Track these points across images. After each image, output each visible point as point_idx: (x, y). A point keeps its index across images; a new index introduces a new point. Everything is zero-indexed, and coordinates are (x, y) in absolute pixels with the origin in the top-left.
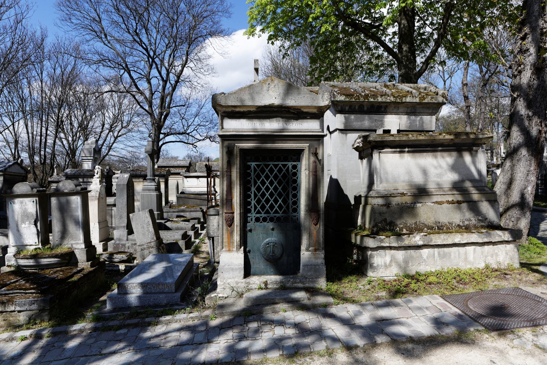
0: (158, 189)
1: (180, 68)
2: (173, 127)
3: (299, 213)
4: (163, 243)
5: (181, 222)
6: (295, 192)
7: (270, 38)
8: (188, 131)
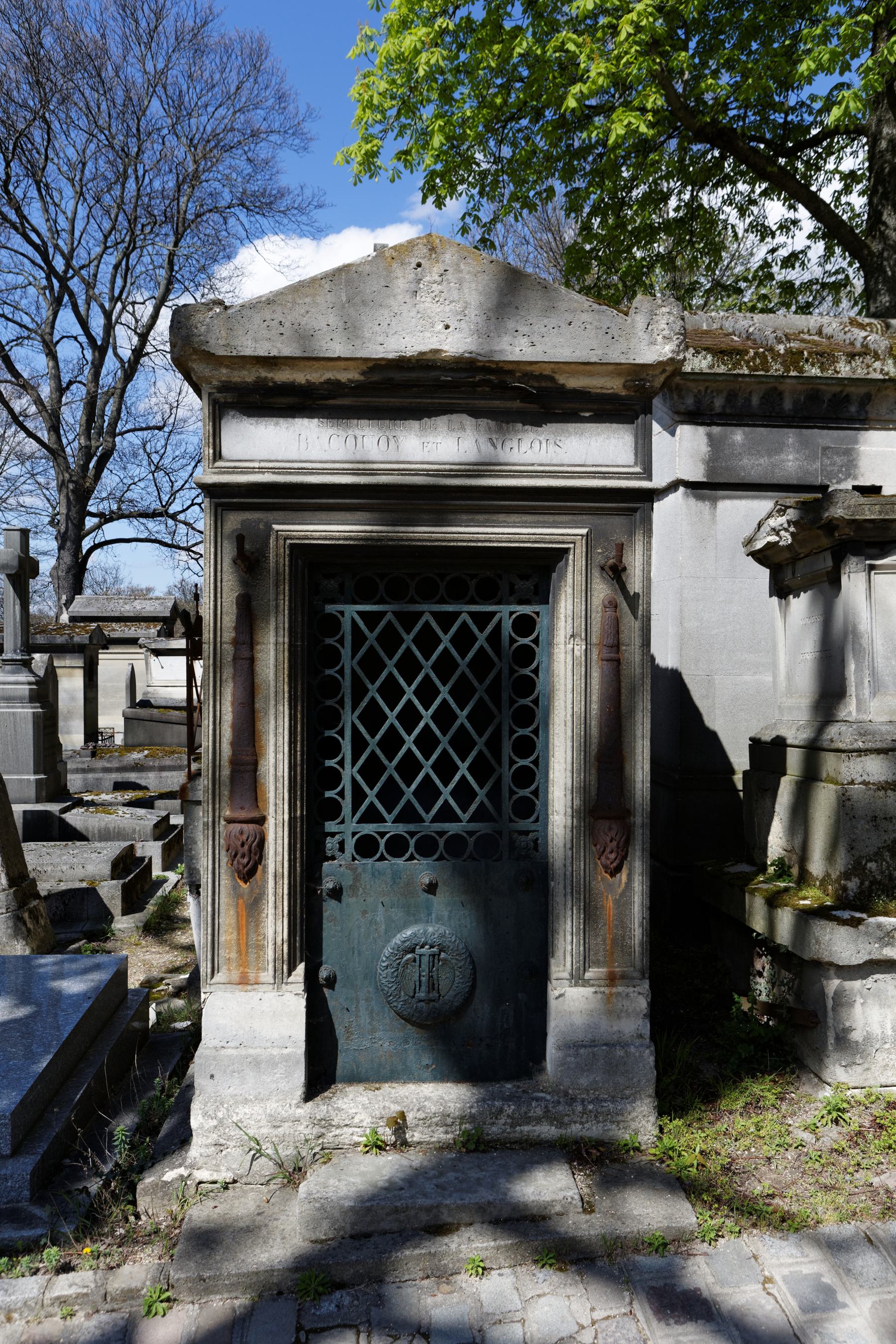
0: (45, 693)
1: (149, 309)
2: (129, 495)
3: (543, 820)
4: (37, 896)
5: (121, 810)
6: (527, 731)
7: (429, 189)
8: (174, 508)
